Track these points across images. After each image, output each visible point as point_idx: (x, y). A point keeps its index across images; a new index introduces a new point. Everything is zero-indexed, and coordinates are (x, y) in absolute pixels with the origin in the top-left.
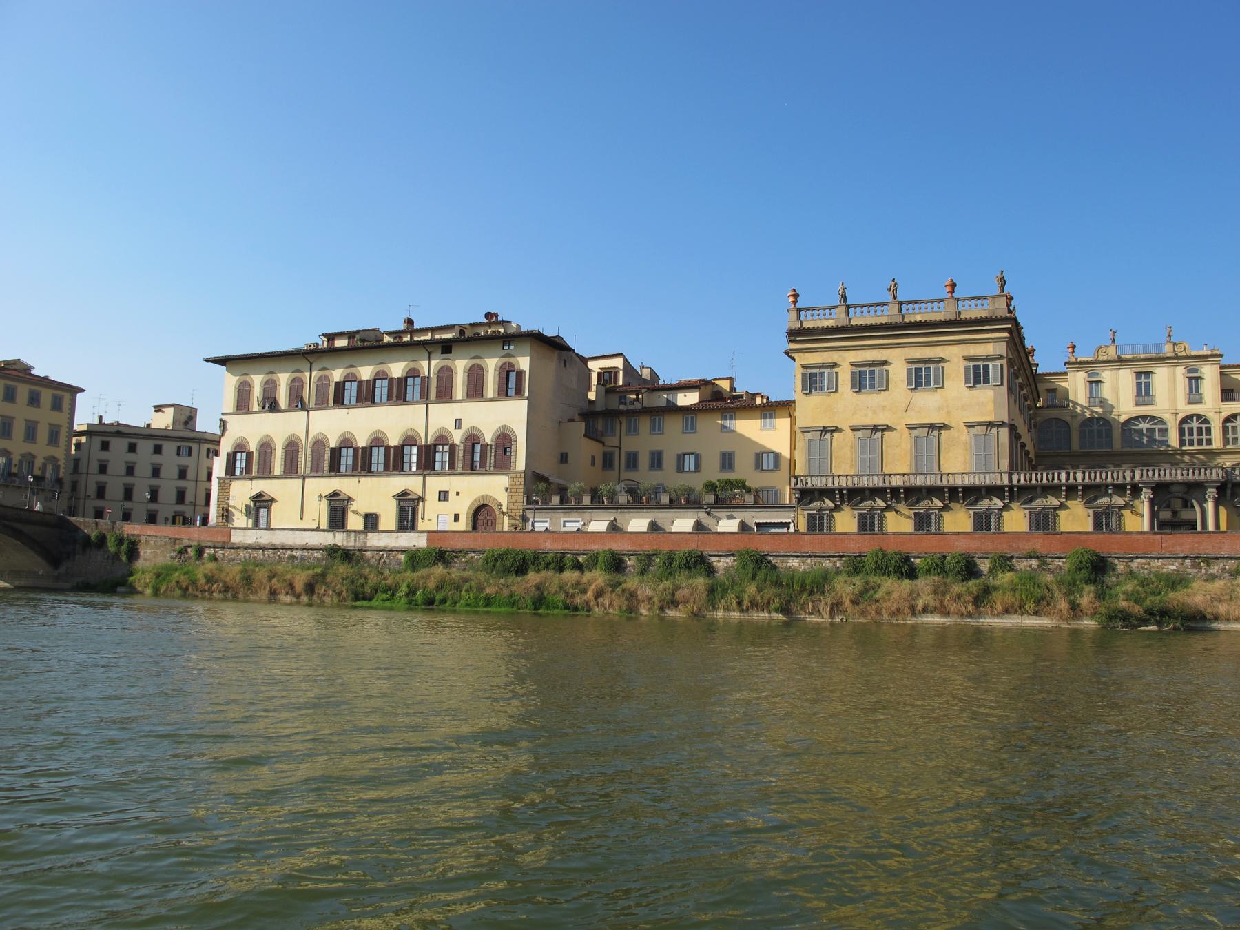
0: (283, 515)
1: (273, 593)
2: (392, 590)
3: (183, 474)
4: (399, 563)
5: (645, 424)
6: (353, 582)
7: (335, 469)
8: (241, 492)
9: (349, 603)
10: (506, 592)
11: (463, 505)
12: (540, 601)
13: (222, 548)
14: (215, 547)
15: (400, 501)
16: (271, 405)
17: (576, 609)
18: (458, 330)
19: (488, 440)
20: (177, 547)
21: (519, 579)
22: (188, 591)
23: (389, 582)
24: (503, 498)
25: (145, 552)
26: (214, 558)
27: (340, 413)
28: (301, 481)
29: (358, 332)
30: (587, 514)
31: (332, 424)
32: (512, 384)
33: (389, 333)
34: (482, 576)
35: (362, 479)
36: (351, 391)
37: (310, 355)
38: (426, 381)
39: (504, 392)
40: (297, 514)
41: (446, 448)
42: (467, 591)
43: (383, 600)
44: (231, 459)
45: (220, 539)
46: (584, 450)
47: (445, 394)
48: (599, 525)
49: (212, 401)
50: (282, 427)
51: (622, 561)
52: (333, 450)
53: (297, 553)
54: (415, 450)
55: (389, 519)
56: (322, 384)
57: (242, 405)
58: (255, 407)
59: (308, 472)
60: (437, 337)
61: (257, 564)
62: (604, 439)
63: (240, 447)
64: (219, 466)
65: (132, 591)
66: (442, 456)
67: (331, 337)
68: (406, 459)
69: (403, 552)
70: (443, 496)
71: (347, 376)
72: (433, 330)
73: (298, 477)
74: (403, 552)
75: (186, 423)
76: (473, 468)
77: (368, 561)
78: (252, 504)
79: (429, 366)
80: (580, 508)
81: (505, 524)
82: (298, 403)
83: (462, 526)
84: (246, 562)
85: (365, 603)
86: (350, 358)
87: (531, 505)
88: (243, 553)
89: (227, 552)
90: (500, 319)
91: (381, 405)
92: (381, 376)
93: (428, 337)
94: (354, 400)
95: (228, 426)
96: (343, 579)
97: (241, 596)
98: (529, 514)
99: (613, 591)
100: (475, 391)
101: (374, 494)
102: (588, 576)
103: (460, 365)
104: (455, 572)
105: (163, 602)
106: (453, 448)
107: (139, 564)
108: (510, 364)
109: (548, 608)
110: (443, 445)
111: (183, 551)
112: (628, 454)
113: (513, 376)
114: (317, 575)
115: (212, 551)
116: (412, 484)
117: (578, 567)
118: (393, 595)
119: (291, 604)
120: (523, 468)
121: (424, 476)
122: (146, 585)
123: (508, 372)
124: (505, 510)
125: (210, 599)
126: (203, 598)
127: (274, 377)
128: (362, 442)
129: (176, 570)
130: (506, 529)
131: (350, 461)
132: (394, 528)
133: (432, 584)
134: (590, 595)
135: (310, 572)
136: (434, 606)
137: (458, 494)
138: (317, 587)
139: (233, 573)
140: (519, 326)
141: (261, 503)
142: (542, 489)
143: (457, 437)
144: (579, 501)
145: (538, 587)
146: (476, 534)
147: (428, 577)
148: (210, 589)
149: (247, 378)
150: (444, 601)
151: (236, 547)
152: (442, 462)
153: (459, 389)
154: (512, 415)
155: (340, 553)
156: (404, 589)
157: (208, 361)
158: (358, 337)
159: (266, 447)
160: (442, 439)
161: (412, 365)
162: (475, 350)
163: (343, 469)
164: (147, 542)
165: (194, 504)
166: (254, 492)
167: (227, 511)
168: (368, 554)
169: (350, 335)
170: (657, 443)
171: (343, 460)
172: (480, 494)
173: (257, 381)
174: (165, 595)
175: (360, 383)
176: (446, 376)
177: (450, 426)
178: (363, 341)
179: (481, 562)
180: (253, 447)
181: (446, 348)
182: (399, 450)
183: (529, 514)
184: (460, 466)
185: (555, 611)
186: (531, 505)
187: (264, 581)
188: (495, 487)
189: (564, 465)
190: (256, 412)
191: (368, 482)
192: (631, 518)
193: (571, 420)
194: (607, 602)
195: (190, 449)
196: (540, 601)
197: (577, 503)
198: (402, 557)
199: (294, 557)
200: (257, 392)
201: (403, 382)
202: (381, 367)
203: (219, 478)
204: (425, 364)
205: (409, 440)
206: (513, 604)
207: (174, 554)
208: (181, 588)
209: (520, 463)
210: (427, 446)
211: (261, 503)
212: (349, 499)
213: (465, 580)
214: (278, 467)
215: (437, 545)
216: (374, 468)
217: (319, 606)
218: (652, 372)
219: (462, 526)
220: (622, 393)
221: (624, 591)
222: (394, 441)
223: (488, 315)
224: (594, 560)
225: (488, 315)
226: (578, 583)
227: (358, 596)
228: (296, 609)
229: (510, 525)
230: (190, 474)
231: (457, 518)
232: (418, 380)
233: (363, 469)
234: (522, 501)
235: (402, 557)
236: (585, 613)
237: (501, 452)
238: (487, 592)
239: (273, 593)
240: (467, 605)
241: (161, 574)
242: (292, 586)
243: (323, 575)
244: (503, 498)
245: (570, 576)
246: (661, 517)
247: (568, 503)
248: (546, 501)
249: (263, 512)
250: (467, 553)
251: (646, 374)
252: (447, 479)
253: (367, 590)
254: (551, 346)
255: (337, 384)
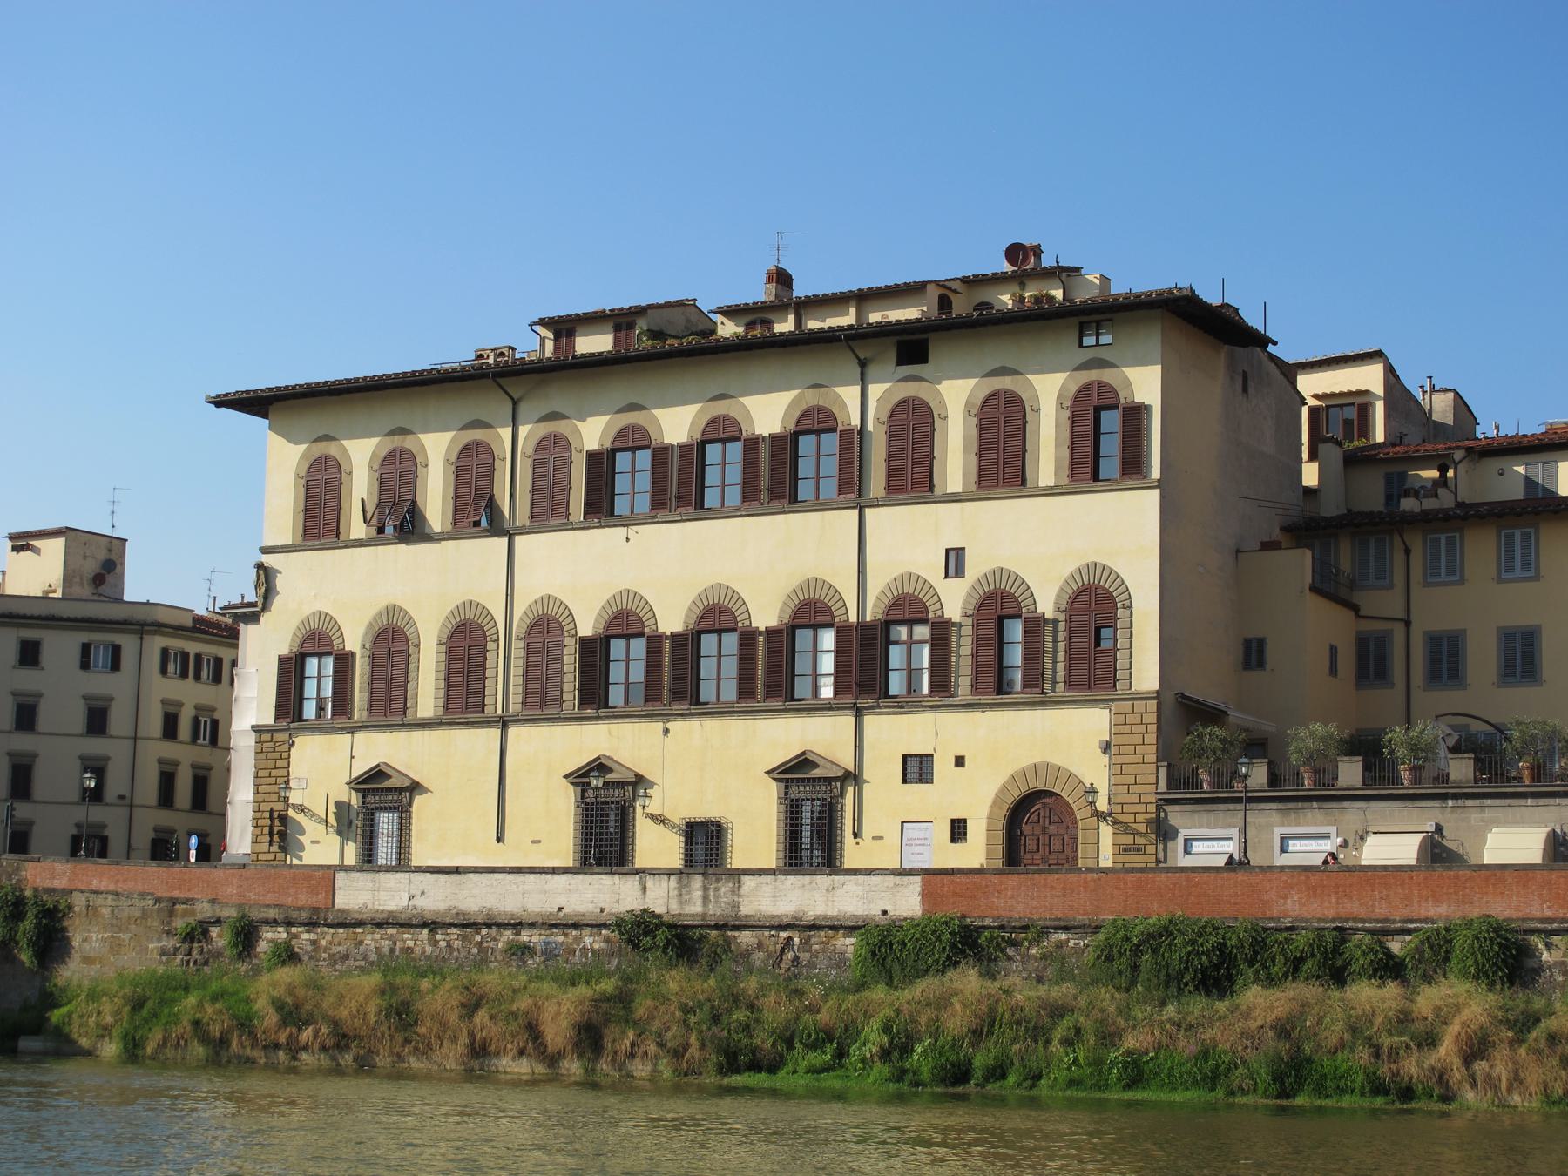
0: (446, 828)
1: (480, 1050)
2: (836, 1043)
3: (97, 720)
4: (840, 961)
5: (1481, 550)
6: (716, 1019)
7: (594, 697)
8: (324, 767)
9: (711, 1079)
10: (1186, 1046)
11: (976, 795)
12: (1293, 1073)
13: (311, 925)
14: (289, 923)
15: (788, 783)
16: (401, 521)
17: (1407, 1093)
18: (933, 294)
19: (1046, 605)
20: (179, 924)
21: (1222, 1006)
22: (228, 1048)
23: (824, 1017)
24: (1095, 771)
25: (86, 939)
26: (287, 955)
27: (607, 538)
28: (495, 733)
29: (641, 311)
30: (1353, 814)
31: (580, 572)
32: (1112, 445)
33: (731, 312)
34: (1107, 998)
35: (676, 726)
36: (633, 476)
37: (500, 378)
38: (853, 442)
39: (1086, 470)
40: (490, 822)
41: (922, 632)
42: (1067, 1042)
43: (813, 1070)
44: (291, 673)
45: (304, 899)
46: (1311, 630)
47: (913, 478)
48: (1392, 845)
49: (205, 525)
50: (436, 582)
51: (1525, 951)
52: (587, 645)
53: (535, 938)
54: (828, 639)
55: (755, 836)
56: (550, 458)
57: (320, 522)
58: (357, 528)
59: (515, 706)
60: (875, 317)
61: (433, 968)
62: (1360, 598)
63: (317, 640)
64: (252, 702)
65: (64, 1048)
66: (910, 655)
67: (564, 328)
68: (802, 664)
69: (851, 930)
70: (917, 768)
71: (622, 433)
72: (863, 298)
73: (488, 723)
74: (851, 930)
75: (98, 580)
76: (1002, 686)
77: (746, 955)
78: (355, 800)
79: (863, 400)
80: (1327, 796)
81: (1105, 847)
82: (478, 513)
83: (975, 853)
84: (388, 963)
85: (761, 1079)
86: (617, 392)
87: (1183, 786)
88: (371, 940)
89: (326, 936)
90: (1047, 261)
91: (724, 513)
92: (721, 431)
93: (848, 319)
94: (643, 503)
95: (280, 582)
96: (687, 1010)
97: (383, 1061)
98: (1175, 816)
99: (1518, 1041)
100: (1002, 466)
101: (717, 767)
102: (1428, 999)
103: (955, 396)
104: (1020, 986)
105: (138, 1079)
106: (942, 632)
107: (71, 973)
108: (1104, 389)
109: (1320, 1090)
110: (911, 623)
111: (197, 934)
112: (1434, 640)
113: (1112, 422)
114: (605, 998)
115: (281, 934)
116: (824, 735)
117: (1389, 968)
118: (841, 1054)
119: (533, 1082)
120: (1155, 686)
121: (859, 714)
122: (105, 1032)
123: (1098, 410)
124: (1102, 805)
125: (293, 1071)
126: (273, 1068)
127: (408, 442)
128: (671, 620)
129: (186, 989)
130: (1106, 860)
131: (638, 673)
132: (569, 861)
133: (957, 1022)
134: (1446, 1051)
135: (582, 990)
136: (971, 1087)
137: (960, 761)
138: (610, 1034)
139: (356, 996)
140: (1105, 280)
141: (382, 796)
142: (1205, 745)
143: (954, 601)
144: (1325, 776)
145: (1283, 1029)
146: (1013, 880)
147: (942, 1003)
148: (292, 1040)
149: (331, 449)
150: (998, 1072)
151: (349, 922)
152: (912, 674)
153: (955, 458)
154: (1117, 535)
155: (661, 936)
156: (872, 1040)
157: (221, 402)
158: (642, 324)
159: (392, 641)
160: (908, 607)
161: (812, 398)
162: (998, 352)
163: (616, 696)
164: (91, 911)
165: (127, 801)
166: (360, 768)
167: (284, 819)
168: (746, 937)
169: (621, 320)
170: (1517, 604)
171: (616, 673)
172: (1025, 761)
173: (361, 455)
174: (160, 1062)
175: (662, 454)
176: (914, 427)
177: (930, 567)
178: (656, 334)
179: (1089, 957)
180: (354, 639)
181: (912, 346)
182: (782, 641)
183: (1175, 816)
184: (963, 681)
185: (1346, 1101)
186: (1183, 786)
187: (452, 1017)
188: (1071, 741)
189: (1254, 675)
190: (360, 543)
191: (690, 732)
192: (1489, 825)
193: (1267, 546)
194: (1502, 1071)
195: (116, 650)
196: (1293, 1073)
197: (1319, 783)
198: (848, 944)
199: (526, 949)
200: (361, 486)
201: (785, 446)
202: (721, 408)
203: (257, 729)
204: (849, 395)
205: (811, 612)
206: (1212, 1080)
207: (170, 943)
208: (205, 1039)
209: (1144, 668)
210: (865, 629)
211: (382, 796)
212: (639, 781)
213: (1058, 1011)
214: (427, 694)
215: (951, 909)
216: (707, 691)
217: (615, 1088)
218: (1460, 404)
219: (975, 853)
220: (1387, 465)
221: (1553, 1039)
222: (765, 615)
223: (1015, 252)
224: (1437, 952)
225: (1015, 252)
226: (1404, 1019)
227: (733, 1060)
228: (551, 1099)
229: (1122, 850)
230: (118, 721)
231: (958, 830)
232: (831, 442)
233: (677, 696)
234: (1152, 779)
235: (848, 944)
236: (1437, 1106)
237: (1085, 640)
238: (1131, 1042)
239: (480, 1050)
240: (1072, 1083)
241: (146, 1003)
242: (533, 1031)
243: (623, 999)
244: (1095, 771)
245: (1371, 997)
246: (1458, 822)
247: (1296, 788)
248: (1226, 779)
249: (386, 822)
250: (1045, 931)
251: (1441, 408)
252: (927, 719)
253: (763, 1040)
254: (1207, 329)
255: (591, 456)
